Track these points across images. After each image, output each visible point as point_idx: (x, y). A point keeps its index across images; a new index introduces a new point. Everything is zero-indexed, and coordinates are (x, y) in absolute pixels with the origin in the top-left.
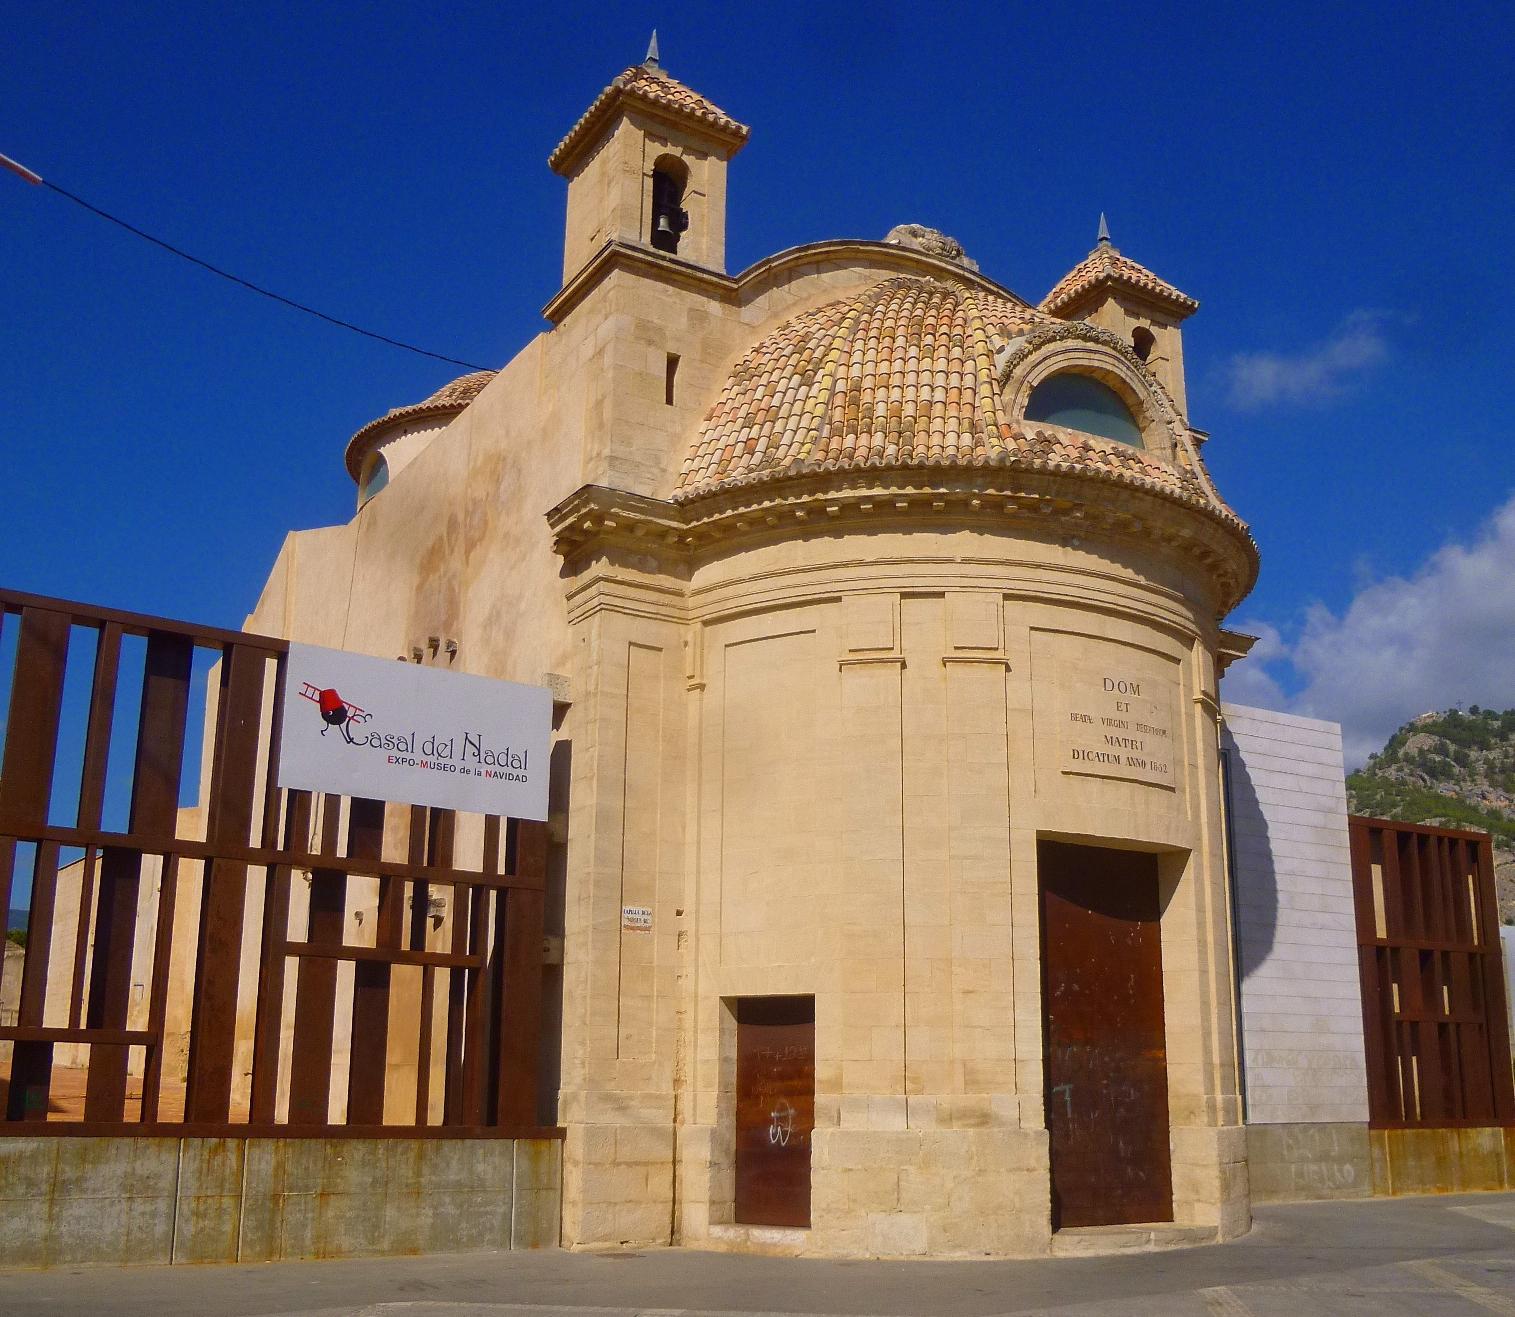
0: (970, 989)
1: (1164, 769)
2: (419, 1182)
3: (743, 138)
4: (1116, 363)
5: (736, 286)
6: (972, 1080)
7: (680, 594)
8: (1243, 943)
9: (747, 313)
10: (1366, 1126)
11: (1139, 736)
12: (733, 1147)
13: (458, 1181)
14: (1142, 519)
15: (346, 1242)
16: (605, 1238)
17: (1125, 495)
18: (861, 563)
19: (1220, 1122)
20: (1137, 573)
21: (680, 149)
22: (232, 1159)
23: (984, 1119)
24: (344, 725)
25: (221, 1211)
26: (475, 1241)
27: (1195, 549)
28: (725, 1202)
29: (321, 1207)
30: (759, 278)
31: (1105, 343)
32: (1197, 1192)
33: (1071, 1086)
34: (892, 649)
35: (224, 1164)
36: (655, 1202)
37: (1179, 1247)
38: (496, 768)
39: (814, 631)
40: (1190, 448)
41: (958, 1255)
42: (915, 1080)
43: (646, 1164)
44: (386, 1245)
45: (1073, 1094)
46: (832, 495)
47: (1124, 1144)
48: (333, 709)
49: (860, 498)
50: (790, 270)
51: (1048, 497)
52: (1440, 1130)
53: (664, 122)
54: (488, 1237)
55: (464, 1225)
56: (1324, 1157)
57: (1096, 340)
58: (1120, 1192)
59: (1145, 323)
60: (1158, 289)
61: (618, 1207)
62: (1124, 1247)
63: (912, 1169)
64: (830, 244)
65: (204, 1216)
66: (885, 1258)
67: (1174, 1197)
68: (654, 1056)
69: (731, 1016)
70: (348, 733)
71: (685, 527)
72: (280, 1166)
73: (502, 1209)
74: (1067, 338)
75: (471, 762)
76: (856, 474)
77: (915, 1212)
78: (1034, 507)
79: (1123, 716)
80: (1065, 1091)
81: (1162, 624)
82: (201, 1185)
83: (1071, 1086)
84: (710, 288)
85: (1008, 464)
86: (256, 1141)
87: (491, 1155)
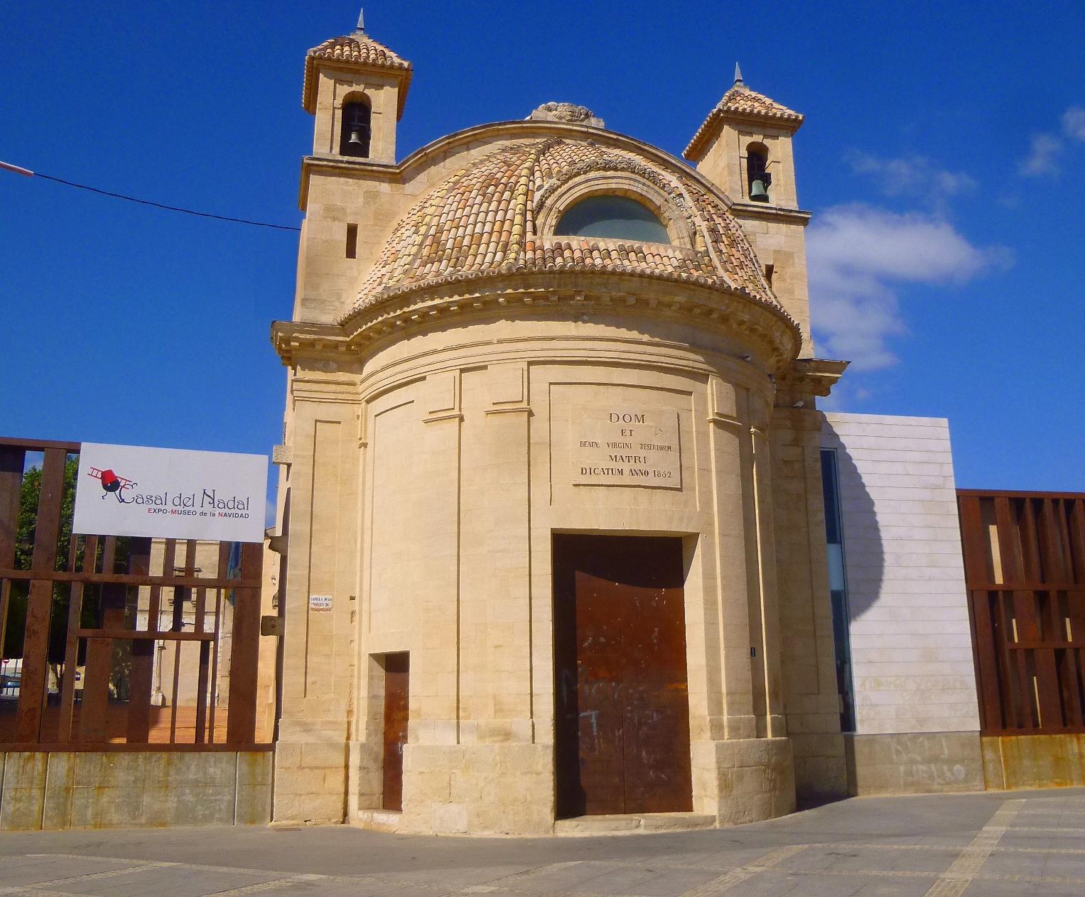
0: (499, 644)
1: (668, 475)
2: (167, 780)
3: (407, 70)
4: (632, 182)
5: (398, 171)
6: (499, 710)
7: (353, 384)
8: (850, 596)
9: (409, 187)
10: (978, 734)
11: (642, 453)
12: (382, 755)
13: (196, 779)
14: (634, 294)
15: (115, 818)
16: (293, 818)
17: (614, 279)
18: (435, 352)
19: (726, 737)
20: (642, 332)
21: (363, 86)
22: (39, 765)
23: (507, 735)
24: (118, 492)
25: (31, 798)
26: (208, 818)
27: (695, 310)
28: (374, 794)
29: (98, 796)
30: (419, 162)
31: (623, 169)
32: (705, 790)
33: (597, 712)
34: (453, 409)
35: (33, 768)
36: (330, 794)
37: (670, 831)
38: (226, 511)
39: (413, 402)
40: (706, 234)
41: (488, 834)
42: (465, 709)
43: (324, 768)
44: (143, 820)
45: (598, 718)
46: (413, 307)
47: (646, 754)
48: (110, 482)
49: (429, 307)
50: (445, 152)
51: (551, 289)
52: (1058, 736)
53: (350, 71)
54: (217, 816)
55: (199, 807)
56: (934, 759)
57: (616, 169)
58: (642, 789)
59: (758, 138)
60: (756, 111)
61: (303, 797)
62: (615, 830)
63: (458, 772)
64: (474, 130)
65: (19, 800)
66: (442, 834)
67: (693, 793)
68: (332, 695)
69: (380, 667)
70: (120, 497)
71: (348, 339)
72: (71, 770)
73: (227, 797)
74: (590, 171)
75: (208, 508)
76: (422, 292)
77: (459, 803)
78: (545, 297)
79: (628, 440)
80: (592, 715)
81: (661, 367)
82: (18, 782)
83: (597, 712)
84: (381, 175)
85: (514, 271)
86: (55, 754)
87: (220, 763)
